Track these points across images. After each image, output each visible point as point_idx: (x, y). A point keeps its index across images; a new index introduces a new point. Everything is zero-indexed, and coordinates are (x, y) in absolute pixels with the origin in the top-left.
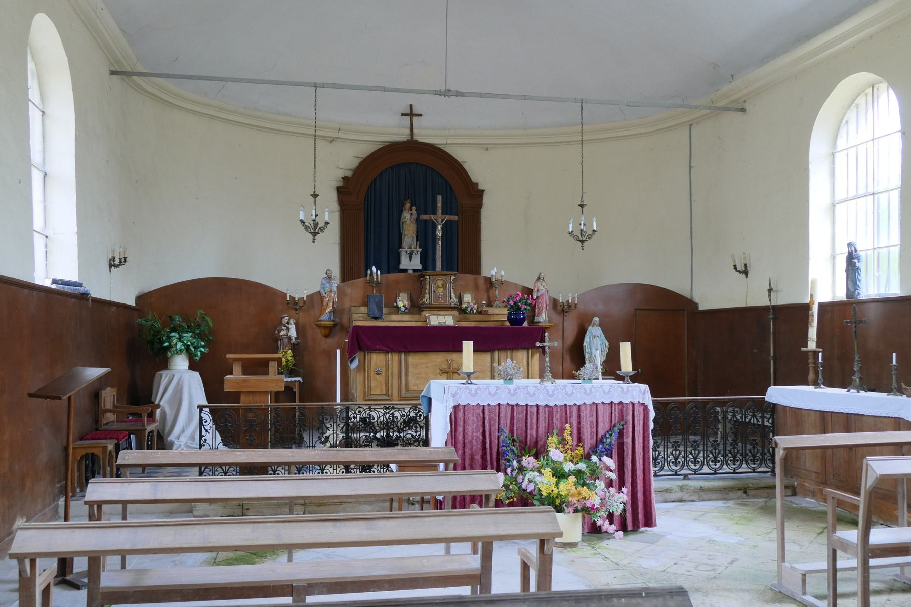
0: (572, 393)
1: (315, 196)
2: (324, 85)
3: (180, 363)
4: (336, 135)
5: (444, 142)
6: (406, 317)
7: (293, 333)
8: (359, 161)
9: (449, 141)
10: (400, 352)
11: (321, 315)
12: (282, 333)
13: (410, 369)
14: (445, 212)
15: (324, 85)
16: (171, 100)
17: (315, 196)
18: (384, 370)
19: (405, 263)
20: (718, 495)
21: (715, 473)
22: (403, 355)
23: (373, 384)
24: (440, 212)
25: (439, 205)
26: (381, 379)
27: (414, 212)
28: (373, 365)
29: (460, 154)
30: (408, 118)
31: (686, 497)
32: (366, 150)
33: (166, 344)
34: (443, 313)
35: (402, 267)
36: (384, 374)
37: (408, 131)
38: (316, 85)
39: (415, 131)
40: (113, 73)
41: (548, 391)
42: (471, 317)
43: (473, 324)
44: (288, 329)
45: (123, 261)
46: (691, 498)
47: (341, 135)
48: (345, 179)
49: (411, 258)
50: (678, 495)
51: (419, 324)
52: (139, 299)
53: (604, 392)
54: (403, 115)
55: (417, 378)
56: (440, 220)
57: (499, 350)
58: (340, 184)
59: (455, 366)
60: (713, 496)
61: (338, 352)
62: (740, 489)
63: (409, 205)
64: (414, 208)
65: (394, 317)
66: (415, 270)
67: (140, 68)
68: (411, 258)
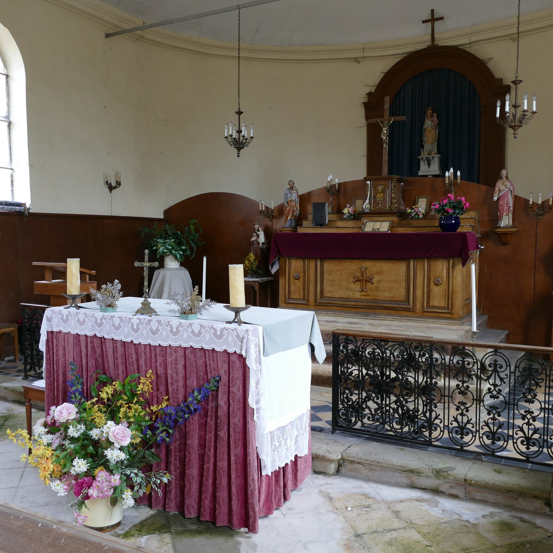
0: (157, 330)
1: (239, 113)
2: (245, 6)
3: (172, 264)
4: (361, 55)
5: (467, 41)
6: (350, 224)
7: (262, 239)
8: (383, 75)
9: (474, 39)
10: (316, 259)
11: (496, 219)
12: (253, 239)
13: (326, 276)
14: (392, 114)
15: (245, 6)
16: (203, 50)
17: (239, 113)
18: (302, 275)
19: (424, 169)
20: (499, 498)
21: (527, 461)
22: (319, 262)
23: (292, 288)
24: (387, 113)
25: (387, 106)
26: (299, 283)
27: (435, 118)
28: (292, 270)
29: (482, 52)
30: (430, 24)
31: (444, 488)
32: (387, 65)
33: (155, 248)
34: (382, 219)
35: (420, 173)
36: (302, 279)
37: (429, 37)
38: (239, 8)
39: (436, 36)
40: (107, 36)
41: (132, 325)
42: (415, 223)
43: (410, 231)
44: (258, 236)
45: (119, 184)
46: (454, 492)
47: (367, 54)
48: (369, 94)
49: (429, 165)
50: (432, 482)
51: (355, 231)
52: (166, 212)
53: (193, 332)
54: (424, 22)
55: (332, 285)
56: (387, 122)
57: (415, 258)
58: (366, 100)
59: (368, 274)
60: (491, 497)
61: (35, 263)
62: (537, 497)
63: (430, 111)
64: (435, 114)
65: (340, 224)
66: (434, 176)
67: (127, 27)
68: (429, 165)
